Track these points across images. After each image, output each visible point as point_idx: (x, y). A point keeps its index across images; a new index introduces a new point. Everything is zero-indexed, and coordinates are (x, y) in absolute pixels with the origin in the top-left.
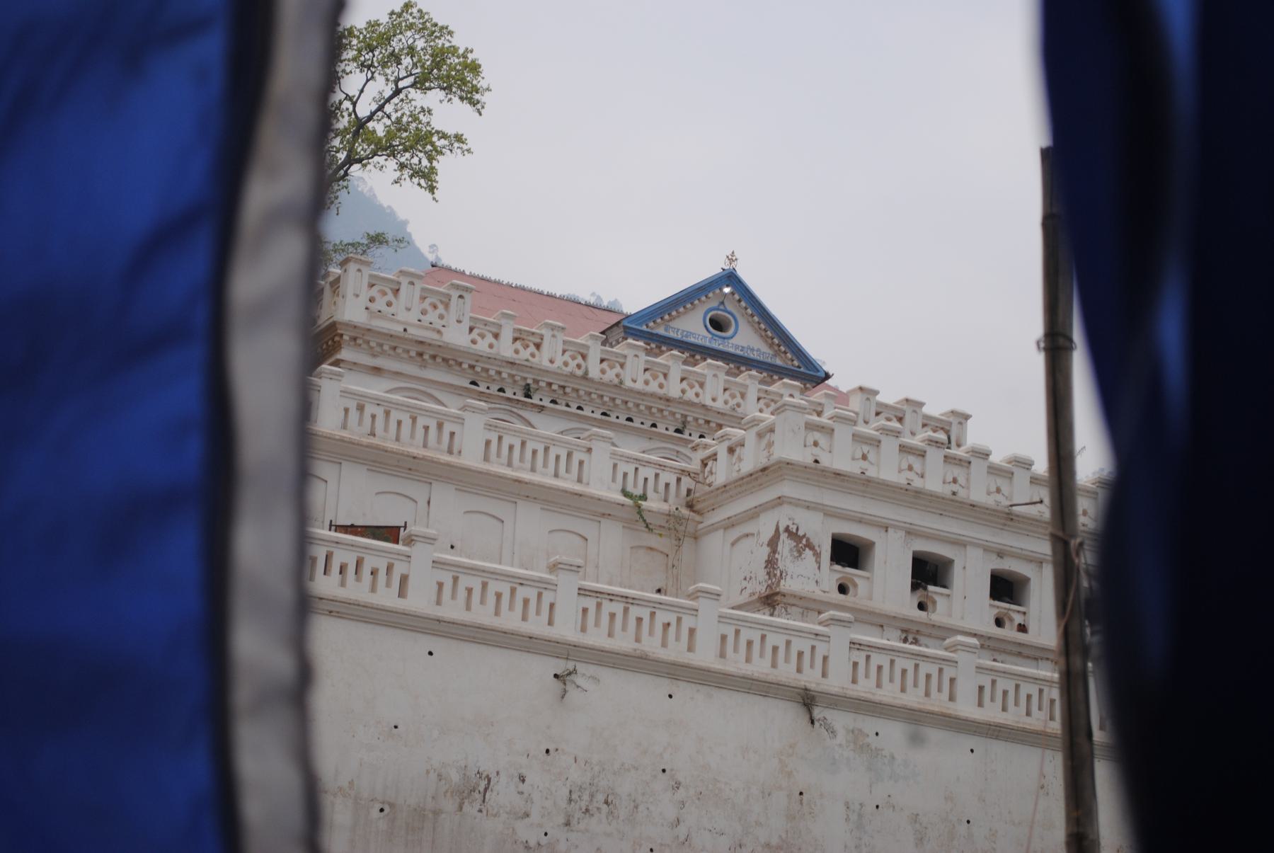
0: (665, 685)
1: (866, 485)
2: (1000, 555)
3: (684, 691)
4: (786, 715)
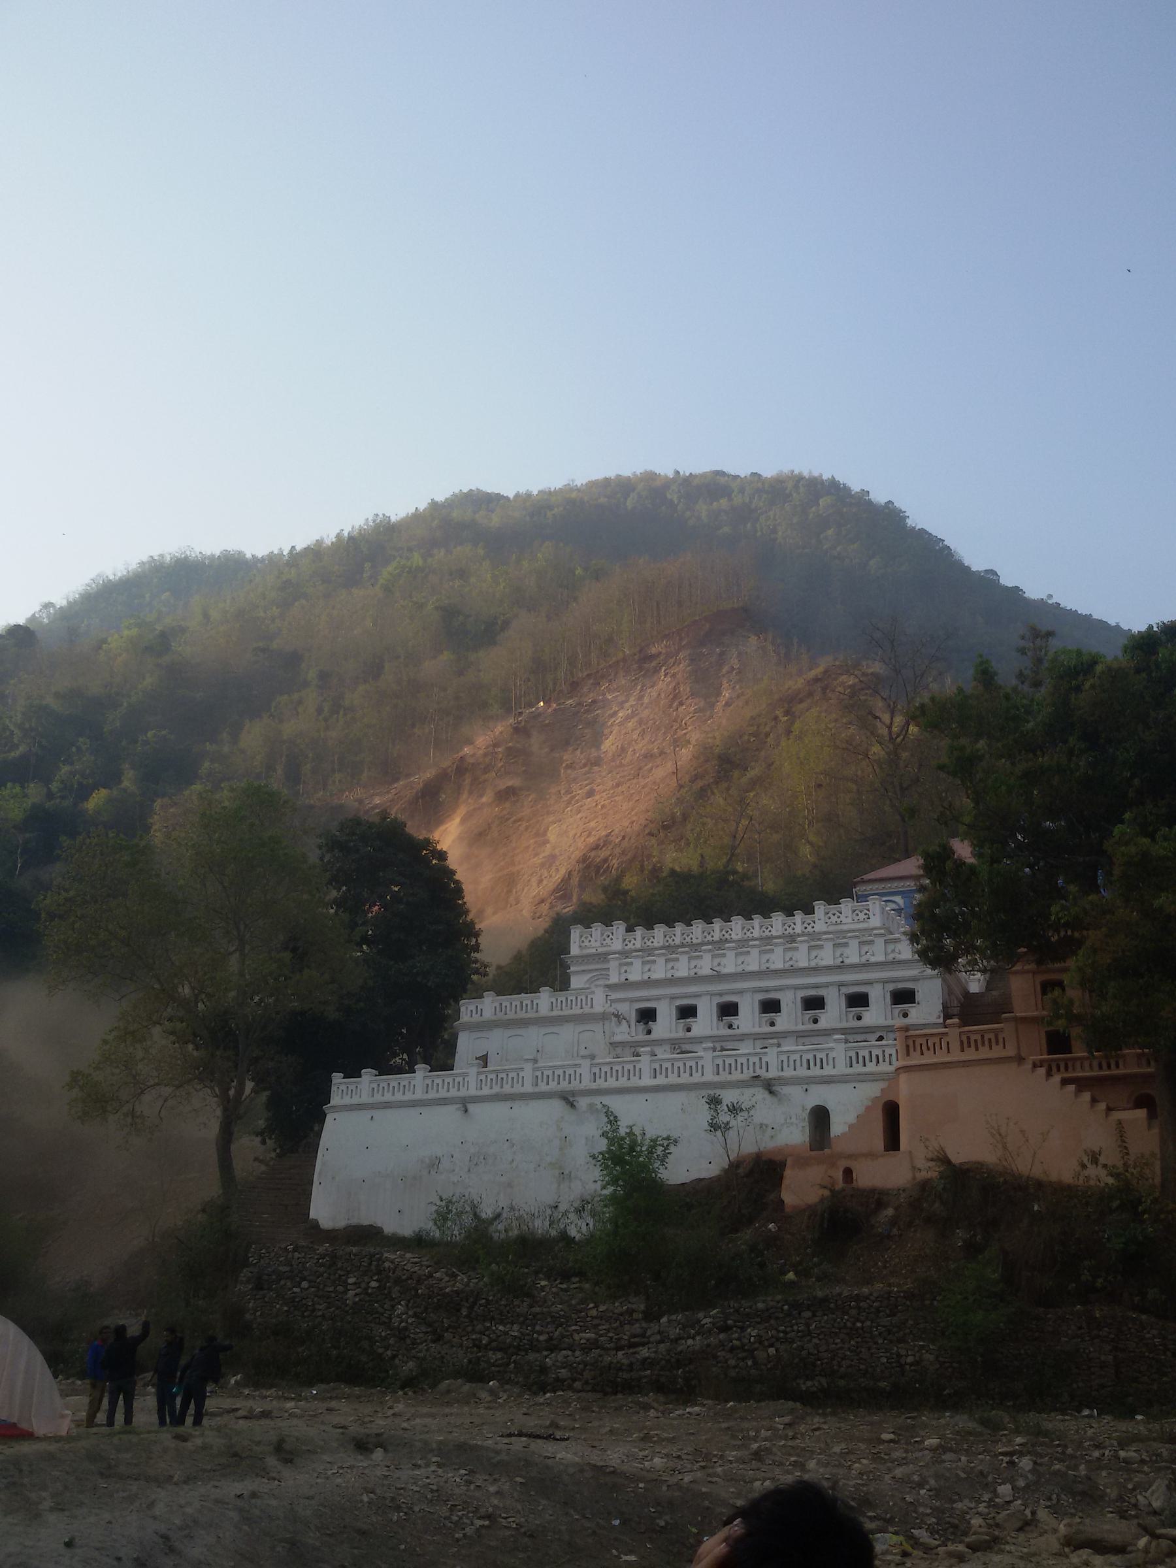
0: (509, 1104)
1: (648, 983)
2: (721, 995)
3: (517, 1105)
4: (557, 1105)
